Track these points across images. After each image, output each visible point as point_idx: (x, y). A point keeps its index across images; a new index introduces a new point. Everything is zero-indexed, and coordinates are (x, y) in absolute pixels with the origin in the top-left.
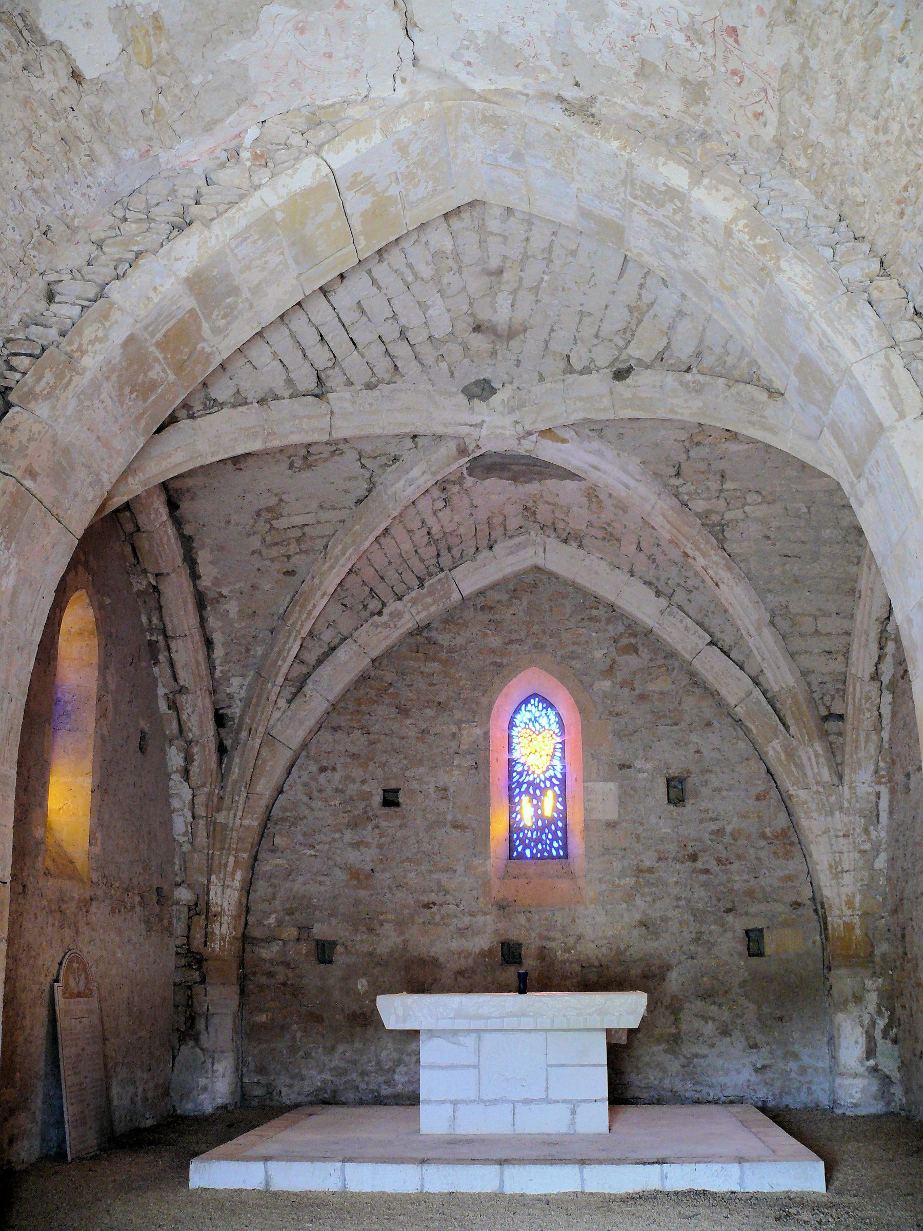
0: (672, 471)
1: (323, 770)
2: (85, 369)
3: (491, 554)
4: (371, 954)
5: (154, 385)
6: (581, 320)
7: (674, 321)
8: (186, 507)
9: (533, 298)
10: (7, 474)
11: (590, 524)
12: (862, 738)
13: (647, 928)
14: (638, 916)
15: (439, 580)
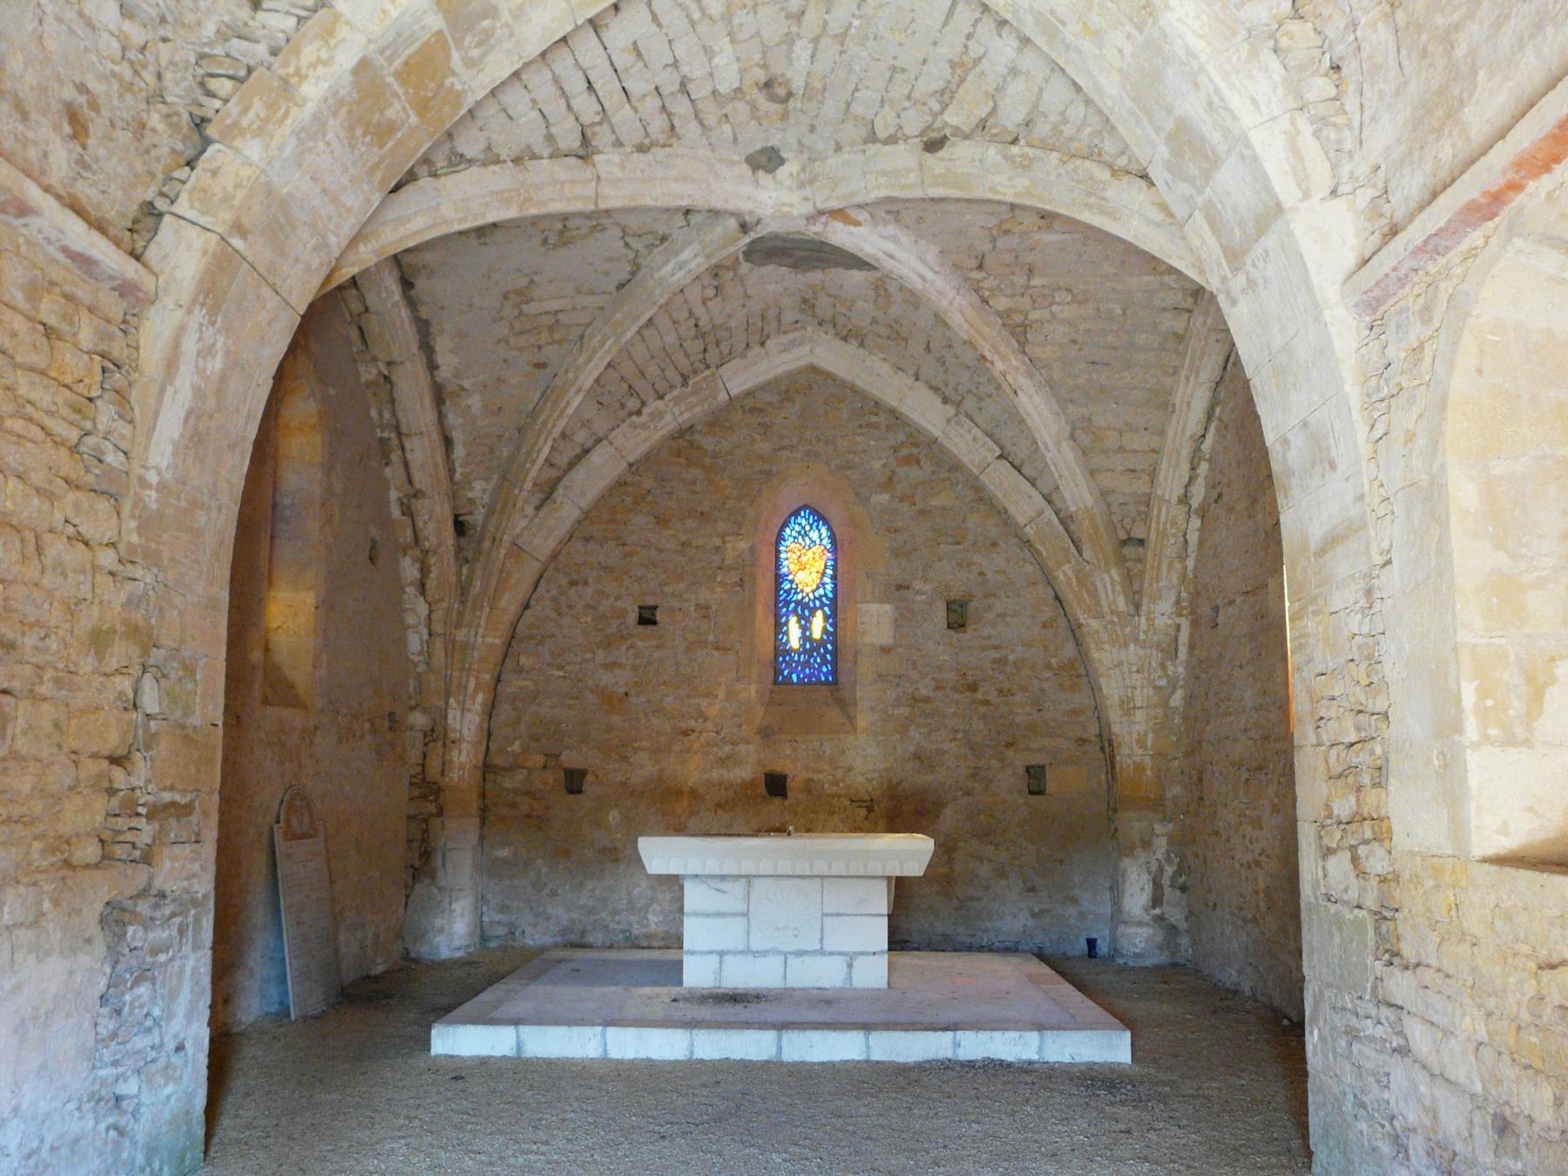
0: (974, 263)
1: (573, 583)
2: (305, 100)
3: (763, 351)
4: (623, 784)
5: (392, 128)
6: (892, 78)
7: (1005, 81)
8: (422, 285)
9: (838, 48)
10: (208, 230)
11: (874, 321)
12: (1164, 565)
13: (922, 762)
14: (912, 749)
15: (706, 378)
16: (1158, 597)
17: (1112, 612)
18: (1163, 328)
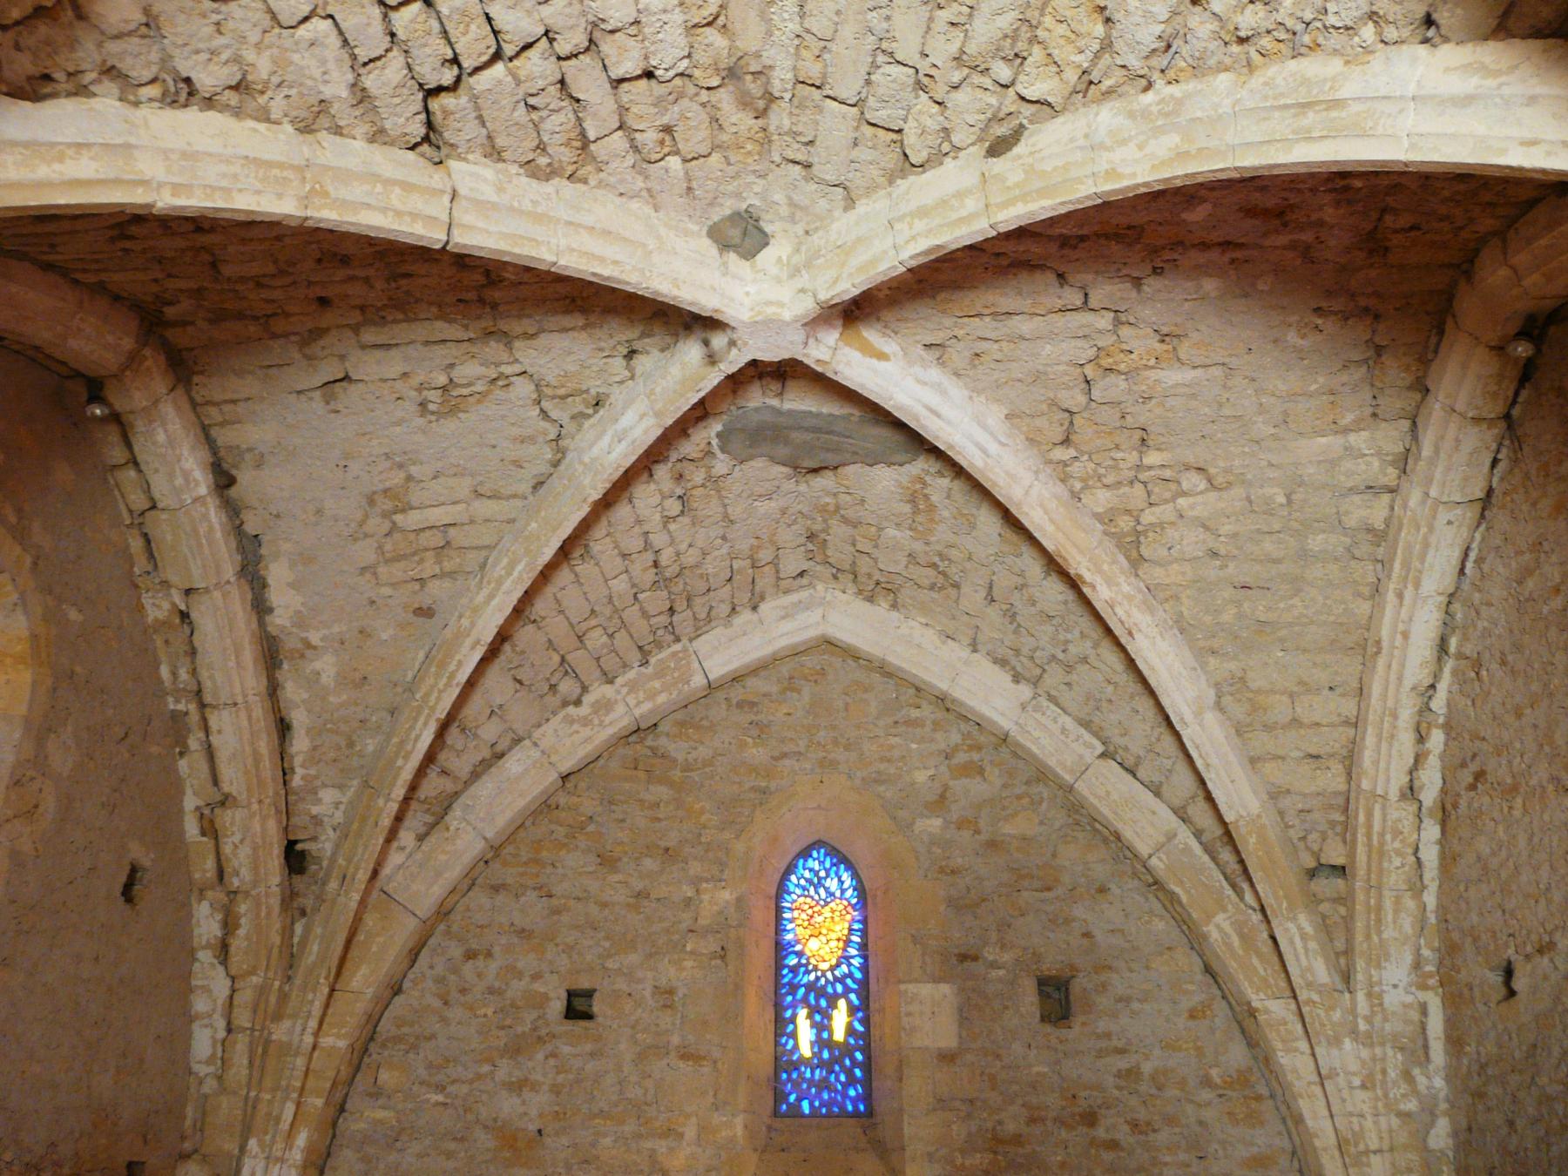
1: (470, 955)
3: (755, 617)
12: (1388, 904)
15: (674, 654)
16: (1379, 958)
17: (1309, 985)
18: (1351, 521)
